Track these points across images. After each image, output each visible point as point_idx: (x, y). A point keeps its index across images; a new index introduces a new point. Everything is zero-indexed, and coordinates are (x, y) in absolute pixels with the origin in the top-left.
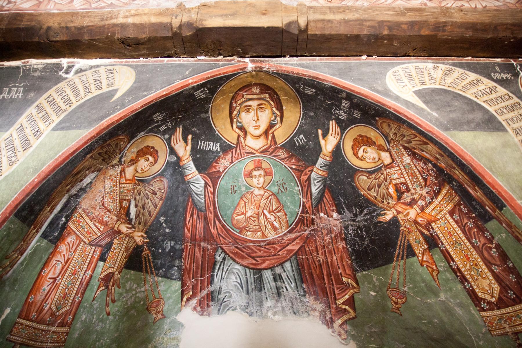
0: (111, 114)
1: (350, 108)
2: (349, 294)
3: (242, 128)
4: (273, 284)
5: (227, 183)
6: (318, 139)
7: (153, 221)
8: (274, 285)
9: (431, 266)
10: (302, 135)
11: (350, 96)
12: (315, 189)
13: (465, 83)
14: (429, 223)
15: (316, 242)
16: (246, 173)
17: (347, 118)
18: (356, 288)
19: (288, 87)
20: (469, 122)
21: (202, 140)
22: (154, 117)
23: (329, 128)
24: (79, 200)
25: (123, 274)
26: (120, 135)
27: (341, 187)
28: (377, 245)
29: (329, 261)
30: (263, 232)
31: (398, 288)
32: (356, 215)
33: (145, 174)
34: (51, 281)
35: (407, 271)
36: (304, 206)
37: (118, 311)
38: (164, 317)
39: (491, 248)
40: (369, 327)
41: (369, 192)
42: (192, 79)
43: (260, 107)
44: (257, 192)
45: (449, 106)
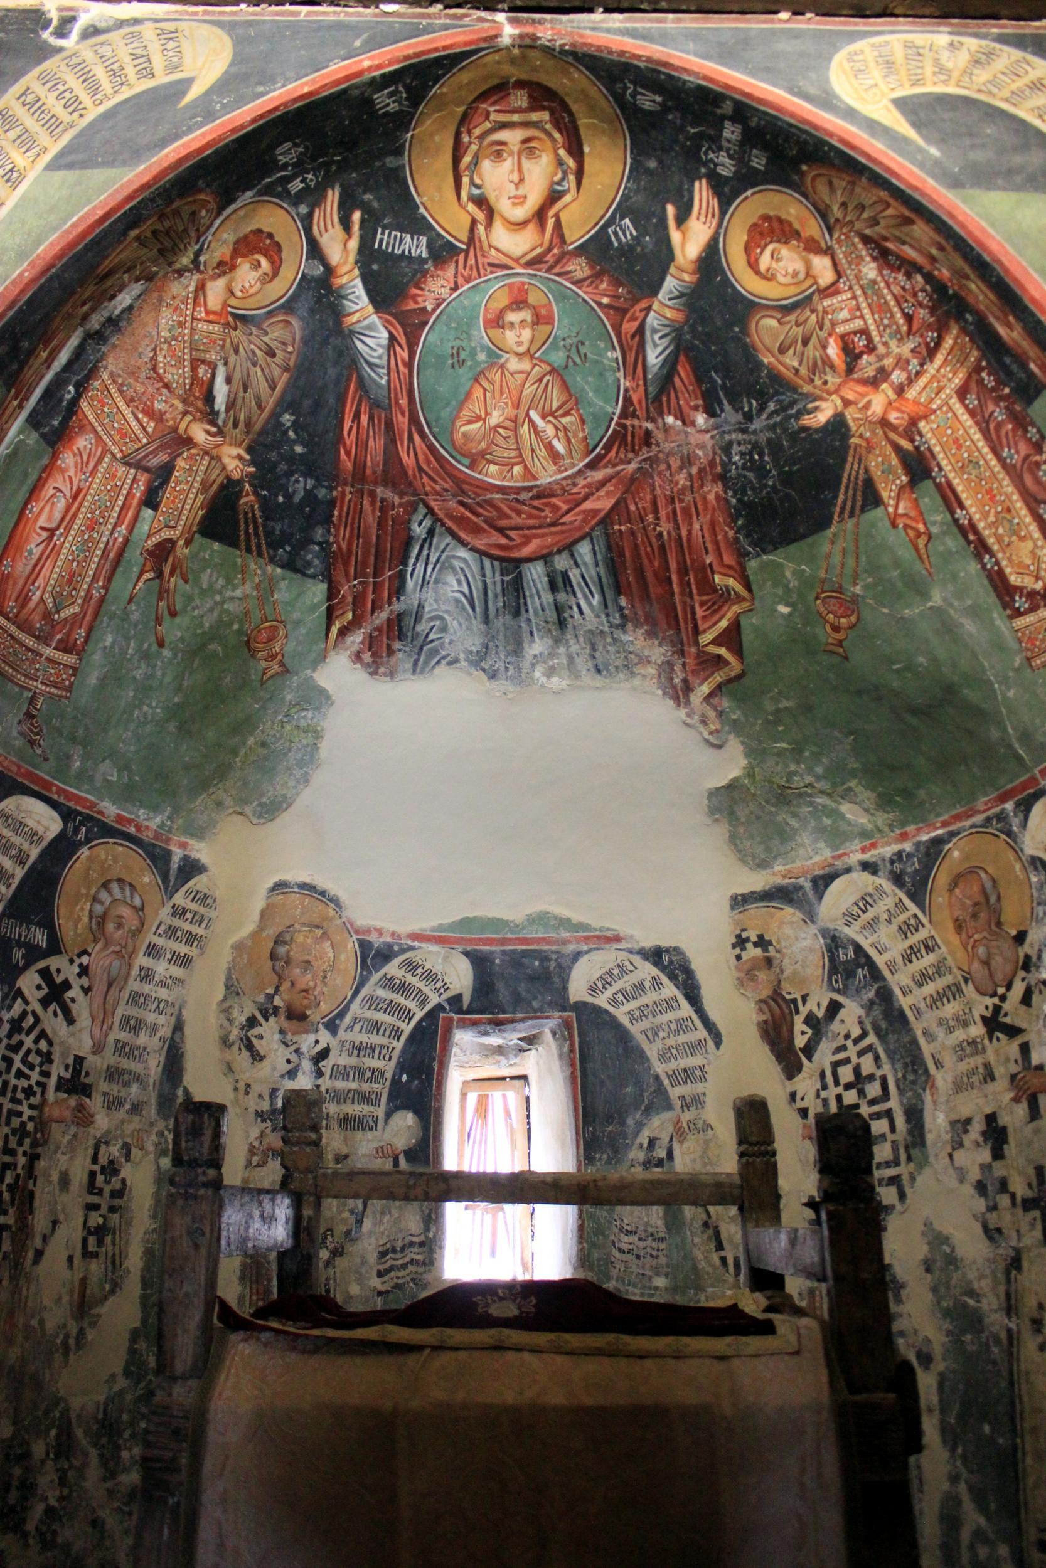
0: (185, 134)
1: (741, 144)
2: (729, 615)
3: (481, 202)
4: (547, 598)
5: (442, 340)
6: (666, 228)
7: (267, 422)
8: (551, 600)
9: (914, 524)
10: (627, 221)
11: (744, 111)
12: (654, 357)
13: (1020, 83)
14: (913, 422)
15: (654, 489)
16: (489, 316)
17: (735, 173)
18: (744, 599)
19: (597, 91)
20: (1010, 172)
21: (384, 228)
22: (279, 150)
23: (691, 200)
24: (103, 349)
25: (195, 545)
26: (200, 191)
27: (717, 346)
28: (798, 486)
29: (684, 533)
30: (526, 467)
31: (840, 590)
32: (749, 417)
33: (252, 303)
34: (45, 534)
35: (862, 543)
36: (628, 400)
37: (182, 640)
38: (286, 671)
39: (1038, 464)
40: (771, 698)
41: (781, 358)
42: (369, 58)
43: (528, 148)
44: (514, 364)
45: (971, 135)
